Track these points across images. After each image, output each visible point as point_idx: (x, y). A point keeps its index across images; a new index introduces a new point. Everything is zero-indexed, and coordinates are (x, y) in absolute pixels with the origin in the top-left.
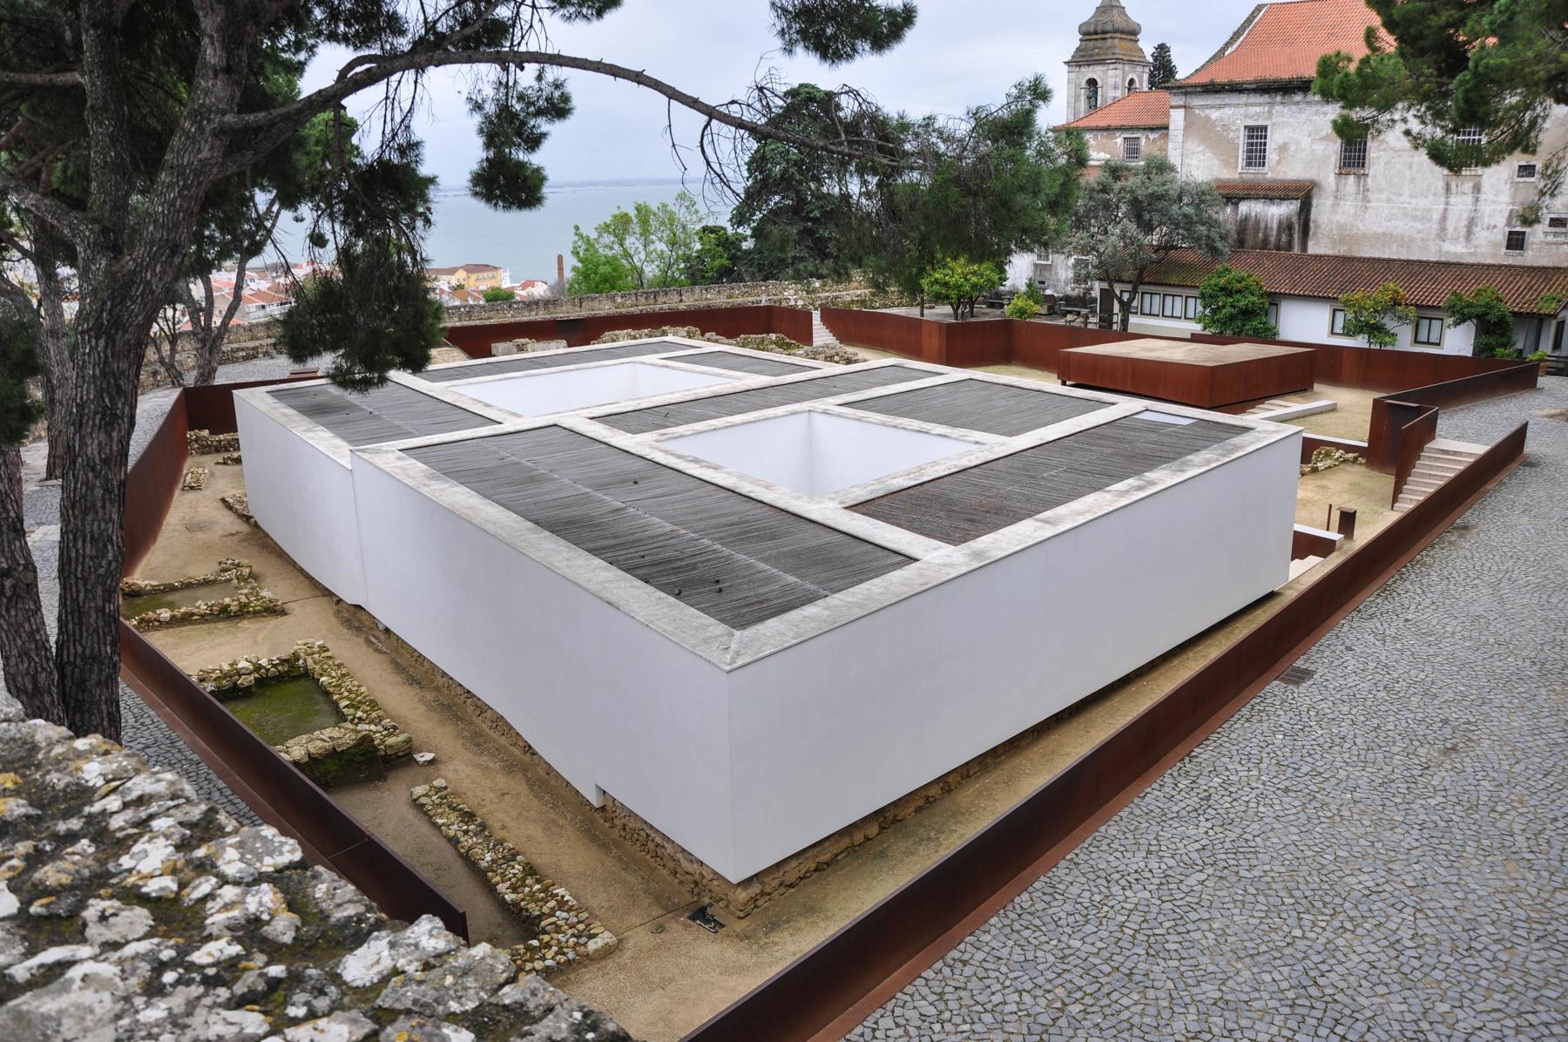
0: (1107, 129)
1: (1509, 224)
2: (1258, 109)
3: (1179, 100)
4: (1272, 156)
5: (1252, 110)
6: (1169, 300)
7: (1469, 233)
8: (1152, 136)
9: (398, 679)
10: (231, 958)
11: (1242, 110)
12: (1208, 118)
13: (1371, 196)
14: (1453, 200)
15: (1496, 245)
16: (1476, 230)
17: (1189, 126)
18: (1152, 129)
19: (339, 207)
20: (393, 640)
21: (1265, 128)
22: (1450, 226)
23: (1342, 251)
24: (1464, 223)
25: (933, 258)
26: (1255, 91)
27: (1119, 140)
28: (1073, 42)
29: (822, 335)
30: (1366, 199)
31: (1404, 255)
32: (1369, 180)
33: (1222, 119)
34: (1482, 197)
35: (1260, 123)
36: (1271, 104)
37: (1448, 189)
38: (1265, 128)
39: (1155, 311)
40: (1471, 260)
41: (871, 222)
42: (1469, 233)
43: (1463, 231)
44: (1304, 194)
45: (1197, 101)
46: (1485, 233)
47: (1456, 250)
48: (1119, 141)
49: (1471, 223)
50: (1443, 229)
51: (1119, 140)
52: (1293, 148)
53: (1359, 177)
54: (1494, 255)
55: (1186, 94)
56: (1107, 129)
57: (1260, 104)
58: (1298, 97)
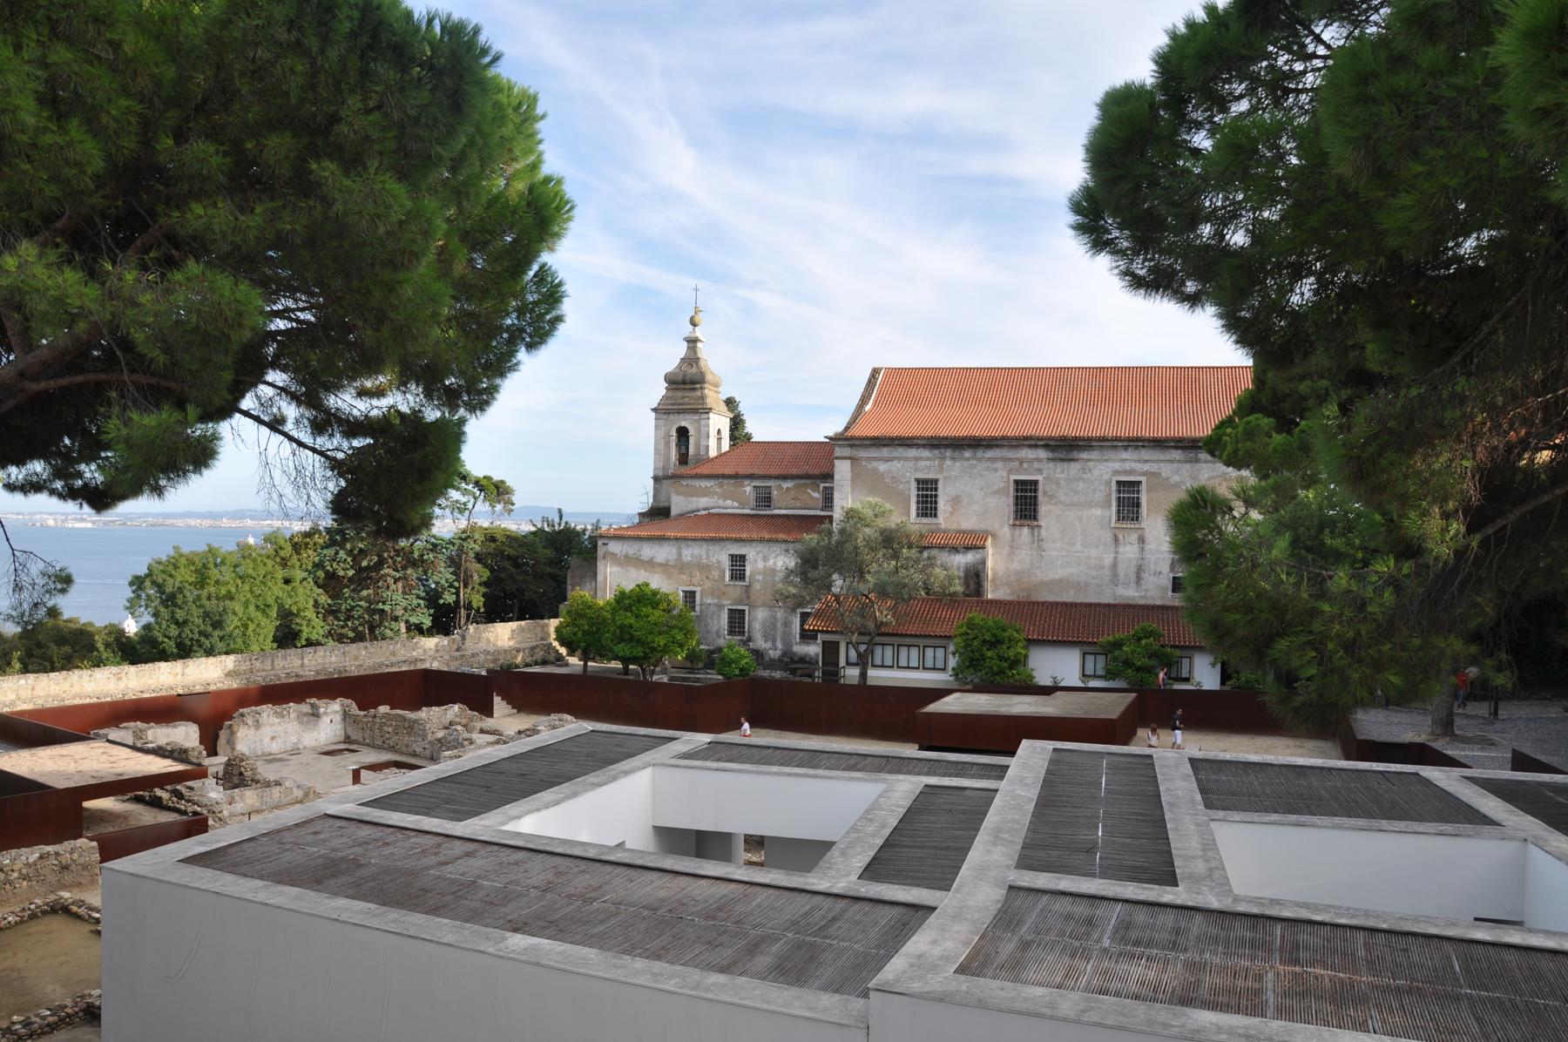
0: (736, 476)
1: (1172, 569)
3: (847, 452)
4: (943, 505)
5: (924, 464)
6: (903, 651)
7: (1139, 579)
8: (786, 485)
10: (299, 403)
12: (875, 470)
13: (1045, 546)
14: (1121, 549)
15: (1164, 589)
16: (1145, 576)
17: (856, 477)
18: (784, 478)
20: (170, 646)
21: (936, 481)
22: (1121, 573)
23: (1022, 596)
24: (1134, 570)
26: (924, 446)
27: (748, 488)
28: (660, 389)
29: (742, 854)
30: (1041, 549)
31: (1081, 599)
32: (1043, 531)
33: (890, 471)
34: (1148, 547)
36: (943, 458)
37: (1116, 539)
38: (936, 481)
39: (914, 663)
40: (1141, 602)
41: (379, 523)
42: (1139, 579)
43: (1133, 577)
44: (973, 542)
45: (863, 453)
46: (1152, 579)
47: (1128, 593)
48: (748, 489)
49: (1139, 571)
50: (1115, 575)
51: (748, 488)
52: (966, 500)
53: (1033, 528)
54: (1162, 598)
56: (736, 476)
58: (967, 454)
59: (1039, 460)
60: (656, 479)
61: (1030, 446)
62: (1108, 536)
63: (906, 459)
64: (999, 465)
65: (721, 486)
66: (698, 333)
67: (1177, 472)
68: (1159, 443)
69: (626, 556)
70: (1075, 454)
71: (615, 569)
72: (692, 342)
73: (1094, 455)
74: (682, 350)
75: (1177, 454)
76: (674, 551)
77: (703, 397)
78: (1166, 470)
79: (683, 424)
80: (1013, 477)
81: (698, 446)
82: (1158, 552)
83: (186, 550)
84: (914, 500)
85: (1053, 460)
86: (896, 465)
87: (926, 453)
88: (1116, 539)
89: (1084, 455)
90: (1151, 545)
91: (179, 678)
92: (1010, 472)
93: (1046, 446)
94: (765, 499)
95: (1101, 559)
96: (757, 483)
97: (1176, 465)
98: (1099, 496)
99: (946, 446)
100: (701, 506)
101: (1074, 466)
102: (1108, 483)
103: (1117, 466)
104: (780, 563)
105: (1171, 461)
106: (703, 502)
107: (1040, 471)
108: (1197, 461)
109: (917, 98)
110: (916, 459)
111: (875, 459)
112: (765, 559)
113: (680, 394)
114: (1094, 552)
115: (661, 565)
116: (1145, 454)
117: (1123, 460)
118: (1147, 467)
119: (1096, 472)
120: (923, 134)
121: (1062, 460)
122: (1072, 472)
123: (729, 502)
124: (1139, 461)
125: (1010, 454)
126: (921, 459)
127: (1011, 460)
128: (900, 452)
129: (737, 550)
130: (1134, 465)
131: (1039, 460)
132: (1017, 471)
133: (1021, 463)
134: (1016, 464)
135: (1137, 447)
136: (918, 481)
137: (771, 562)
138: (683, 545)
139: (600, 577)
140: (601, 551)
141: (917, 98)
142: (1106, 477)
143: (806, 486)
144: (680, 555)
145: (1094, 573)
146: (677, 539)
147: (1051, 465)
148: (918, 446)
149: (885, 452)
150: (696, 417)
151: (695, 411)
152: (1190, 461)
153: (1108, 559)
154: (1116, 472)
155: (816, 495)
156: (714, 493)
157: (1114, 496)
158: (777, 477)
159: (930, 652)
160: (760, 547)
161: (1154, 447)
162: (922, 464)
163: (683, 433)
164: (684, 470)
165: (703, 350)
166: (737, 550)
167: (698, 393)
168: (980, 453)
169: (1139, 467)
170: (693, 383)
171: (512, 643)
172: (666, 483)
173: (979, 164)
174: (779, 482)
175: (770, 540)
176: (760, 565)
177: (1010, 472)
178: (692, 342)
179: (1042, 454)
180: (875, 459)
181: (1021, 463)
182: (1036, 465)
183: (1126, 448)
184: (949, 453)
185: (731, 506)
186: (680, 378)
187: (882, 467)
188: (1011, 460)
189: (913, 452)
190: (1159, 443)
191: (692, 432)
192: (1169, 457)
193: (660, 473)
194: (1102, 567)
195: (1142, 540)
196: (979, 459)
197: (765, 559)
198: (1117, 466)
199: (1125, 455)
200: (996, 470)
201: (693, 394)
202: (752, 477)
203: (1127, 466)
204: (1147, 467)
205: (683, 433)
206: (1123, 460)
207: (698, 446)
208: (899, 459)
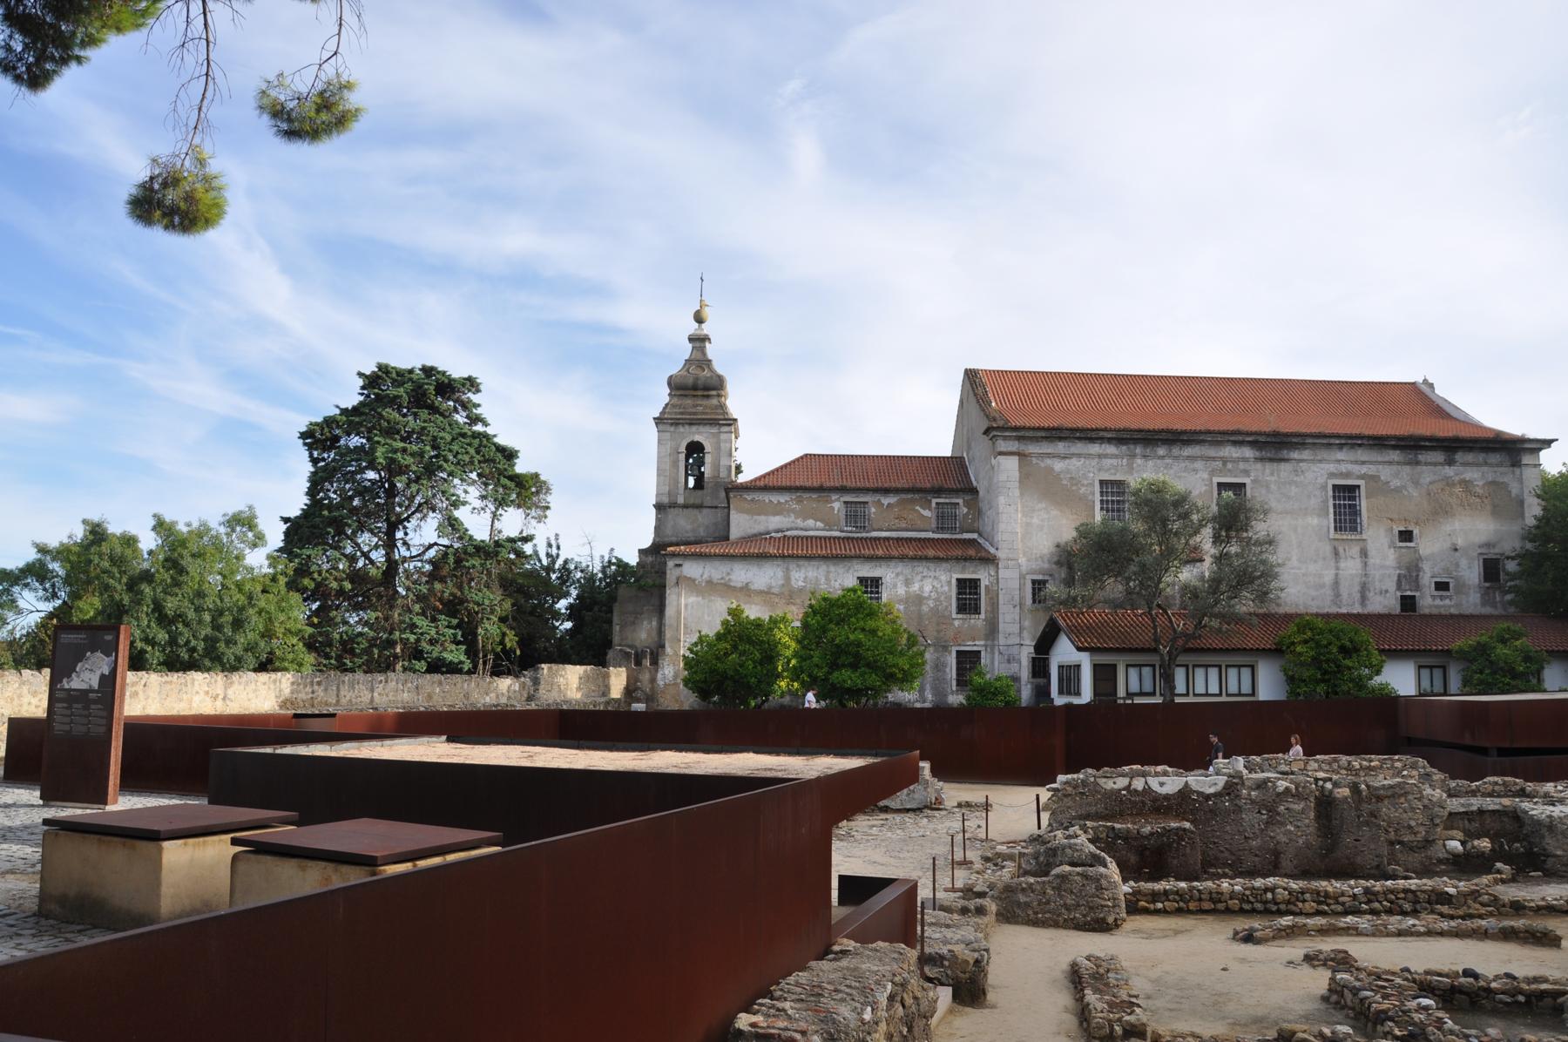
1: (1399, 587)
2: (1114, 462)
8: (886, 501)
9: (335, 134)
11: (1094, 462)
12: (1050, 470)
14: (1342, 565)
16: (1370, 595)
17: (1025, 477)
18: (886, 491)
19: (207, 663)
24: (1357, 588)
25: (749, 687)
26: (1110, 440)
28: (662, 395)
34: (1371, 561)
35: (1118, 477)
36: (1134, 456)
37: (1336, 553)
43: (1357, 596)
45: (1032, 448)
46: (1379, 598)
48: (836, 505)
51: (837, 505)
55: (1019, 438)
57: (1116, 457)
58: (1161, 451)
59: (1245, 460)
60: (659, 507)
61: (1235, 443)
62: (1328, 549)
63: (1089, 456)
64: (1199, 464)
65: (799, 501)
66: (706, 329)
67: (1396, 475)
68: (1379, 442)
69: (710, 582)
70: (1285, 454)
71: (693, 599)
72: (699, 341)
73: (1306, 454)
74: (687, 349)
75: (1395, 455)
76: (780, 573)
77: (722, 407)
78: (1385, 473)
79: (697, 438)
80: (1216, 480)
81: (716, 467)
82: (1383, 567)
83: (53, 542)
84: (1098, 506)
85: (1262, 459)
86: (1075, 464)
87: (1111, 449)
88: (1336, 553)
89: (1295, 455)
90: (1374, 559)
91: (219, 703)
92: (1213, 473)
93: (1254, 444)
94: (855, 515)
95: (1320, 576)
96: (849, 498)
97: (1395, 468)
98: (1314, 502)
99: (1136, 441)
100: (772, 527)
101: (1285, 468)
102: (1324, 487)
103: (1332, 467)
104: (928, 588)
105: (1390, 463)
106: (774, 522)
107: (1246, 473)
108: (1418, 463)
109: (516, 239)
110: (1100, 456)
111: (1049, 455)
112: (907, 583)
113: (689, 401)
114: (1312, 568)
115: (761, 592)
116: (1361, 454)
117: (1339, 461)
118: (1364, 469)
119: (1310, 475)
120: (523, 276)
121: (1271, 460)
122: (1283, 474)
123: (811, 522)
124: (1356, 462)
125: (1211, 452)
126: (1106, 456)
127: (1214, 459)
128: (1079, 447)
129: (869, 571)
130: (1350, 467)
131: (1245, 460)
132: (1220, 472)
133: (1225, 463)
134: (1219, 464)
135: (1353, 446)
136: (1102, 482)
137: (916, 587)
138: (792, 565)
139: (670, 611)
140: (672, 574)
141: (516, 239)
142: (1321, 480)
143: (912, 501)
144: (787, 578)
145: (1313, 593)
146: (783, 557)
147: (1259, 465)
148: (1102, 440)
149: (1061, 447)
150: (715, 430)
151: (714, 422)
152: (1409, 463)
153: (1328, 577)
154: (1332, 475)
155: (927, 513)
156: (790, 511)
157: (1331, 502)
158: (876, 490)
159: (1233, 673)
160: (900, 567)
161: (1371, 446)
162: (1108, 462)
163: (695, 449)
164: (697, 497)
165: (711, 350)
166: (869, 571)
167: (714, 401)
168: (1176, 451)
169: (1356, 469)
170: (707, 388)
171: (579, 696)
172: (672, 512)
173: (583, 311)
174: (877, 497)
175: (914, 558)
176: (901, 590)
177: (1213, 473)
178: (699, 341)
179: (1248, 452)
180: (1049, 455)
181: (1225, 463)
182: (1242, 466)
183: (1341, 446)
184: (1138, 450)
185: (813, 527)
186: (690, 381)
187: (1058, 466)
188: (1214, 459)
189: (1095, 448)
190: (1379, 442)
191: (708, 448)
192: (1387, 459)
193: (666, 500)
194: (1322, 586)
195: (1364, 553)
196: (1176, 458)
197: (907, 583)
198: (1332, 467)
199: (1340, 455)
200: (1196, 471)
201: (705, 402)
202: (843, 490)
203: (1343, 468)
204: (1364, 469)
205: (695, 449)
206: (1339, 461)
207: (716, 467)
208: (1079, 456)
